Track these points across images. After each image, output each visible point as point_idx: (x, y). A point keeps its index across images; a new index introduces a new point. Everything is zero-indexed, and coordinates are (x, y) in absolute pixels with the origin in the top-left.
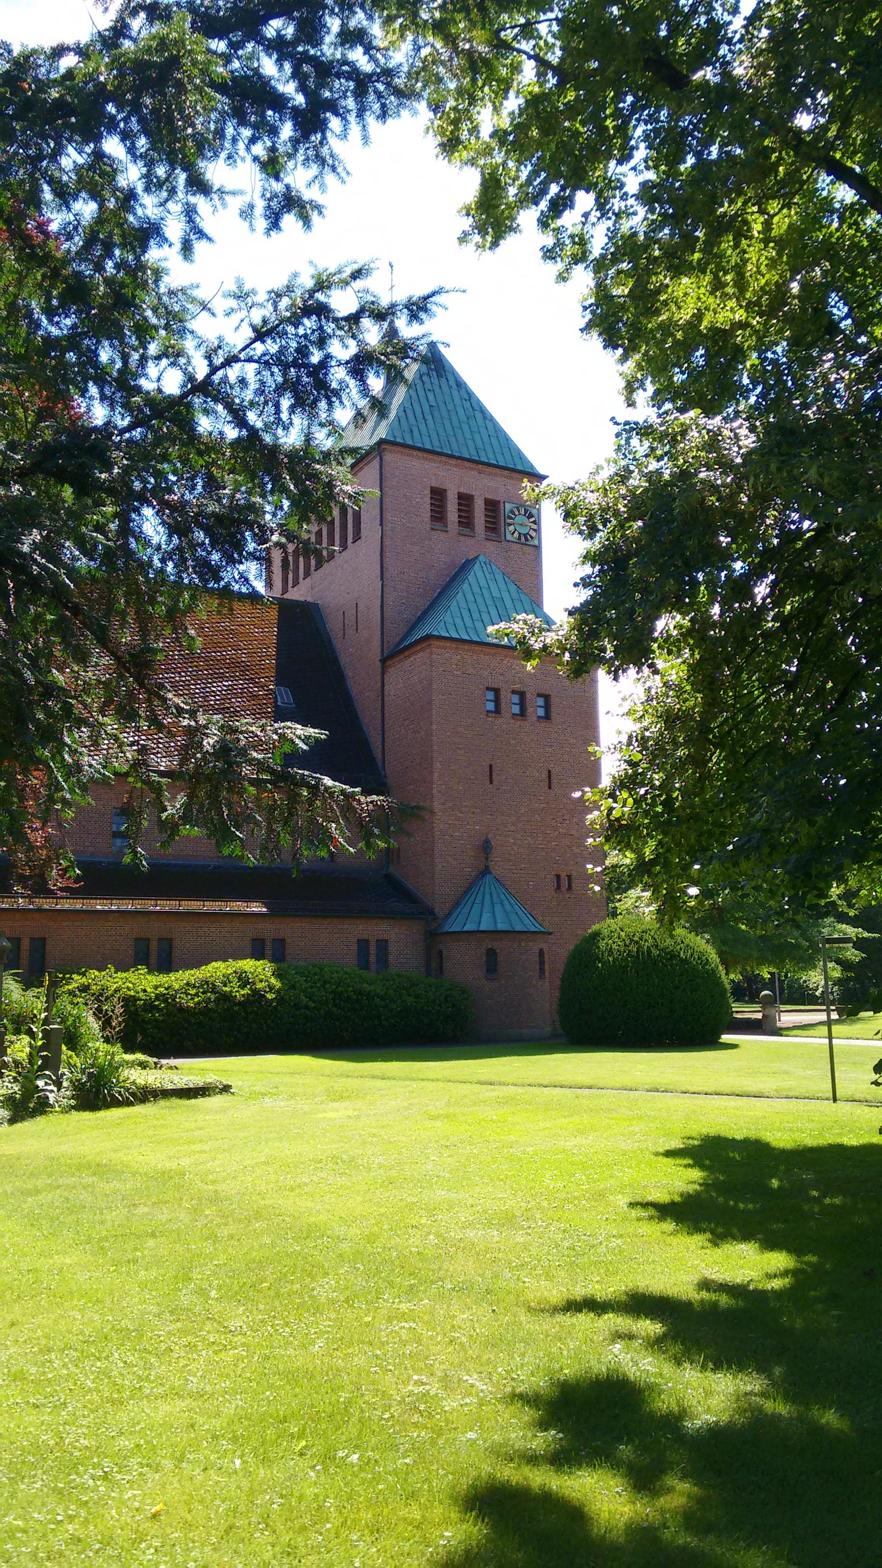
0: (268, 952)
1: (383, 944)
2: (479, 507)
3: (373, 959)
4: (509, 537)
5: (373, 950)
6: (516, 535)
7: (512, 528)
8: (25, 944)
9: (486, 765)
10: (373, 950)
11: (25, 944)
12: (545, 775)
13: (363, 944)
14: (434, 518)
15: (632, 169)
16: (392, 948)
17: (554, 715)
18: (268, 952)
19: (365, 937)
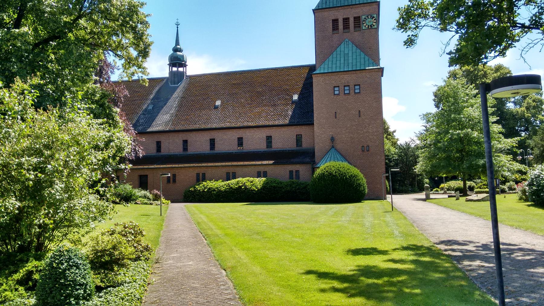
0: (262, 175)
1: (297, 171)
2: (352, 21)
3: (294, 176)
4: (364, 28)
5: (294, 174)
6: (367, 26)
7: (365, 25)
8: (201, 175)
9: (334, 112)
10: (294, 174)
11: (201, 175)
12: (357, 113)
13: (291, 172)
14: (334, 30)
15: (20, 282)
16: (301, 173)
17: (181, 143)
18: (262, 175)
19: (291, 170)
